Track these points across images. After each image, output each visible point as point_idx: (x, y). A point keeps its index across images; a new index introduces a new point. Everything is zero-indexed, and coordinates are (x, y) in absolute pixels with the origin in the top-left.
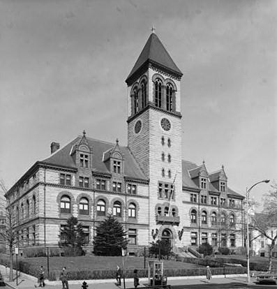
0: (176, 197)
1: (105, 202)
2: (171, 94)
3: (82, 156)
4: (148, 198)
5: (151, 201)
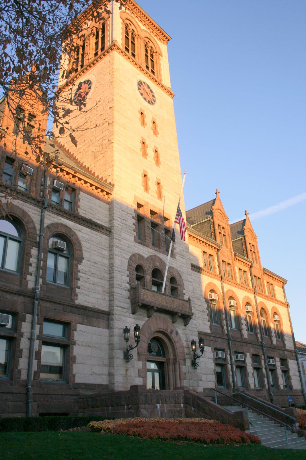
5: (116, 242)
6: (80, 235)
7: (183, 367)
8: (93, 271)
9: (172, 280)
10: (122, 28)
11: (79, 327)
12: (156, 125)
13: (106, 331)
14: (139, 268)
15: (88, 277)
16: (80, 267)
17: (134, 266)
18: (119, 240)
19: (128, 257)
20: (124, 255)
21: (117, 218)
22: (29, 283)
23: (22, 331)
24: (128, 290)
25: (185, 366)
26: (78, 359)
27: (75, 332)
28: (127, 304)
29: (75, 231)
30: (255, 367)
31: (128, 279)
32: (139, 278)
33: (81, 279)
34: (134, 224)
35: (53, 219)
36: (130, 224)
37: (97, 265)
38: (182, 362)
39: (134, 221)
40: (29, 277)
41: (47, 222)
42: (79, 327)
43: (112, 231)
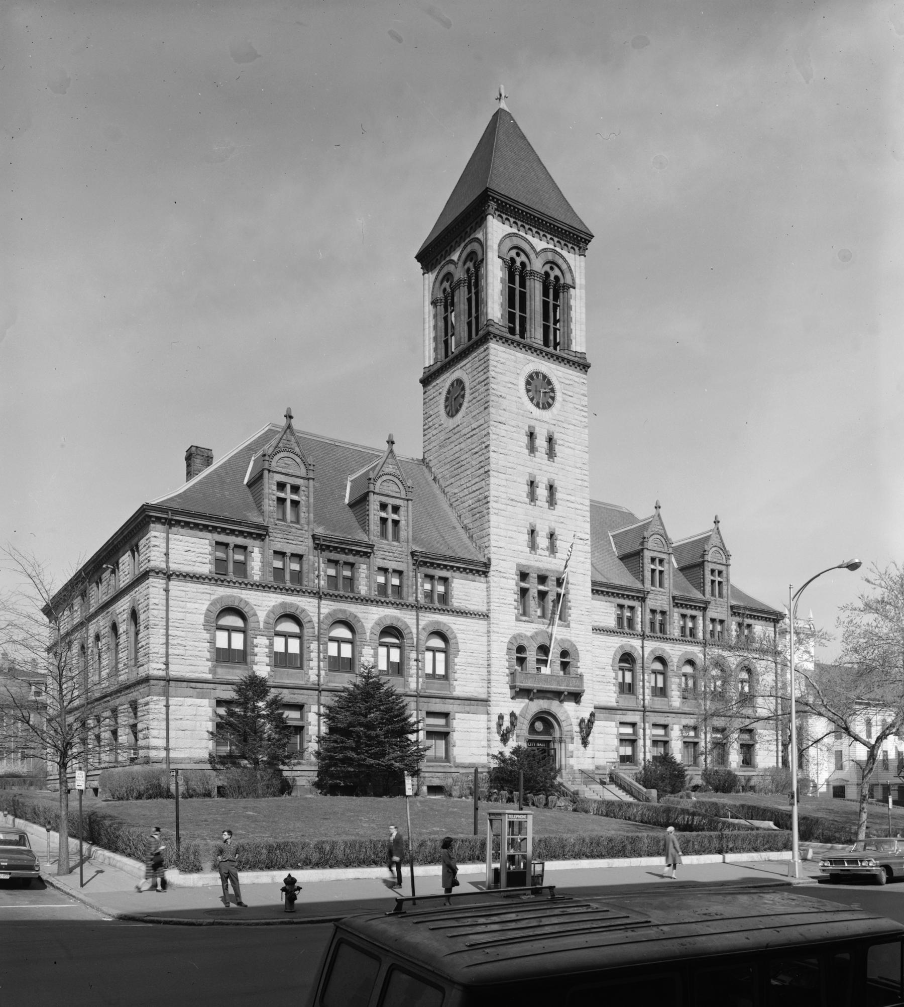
0: (574, 614)
1: (243, 617)
2: (556, 297)
3: (281, 486)
4: (486, 616)
5: (493, 628)
6: (454, 627)
7: (570, 745)
8: (470, 661)
9: (564, 654)
10: (502, 280)
11: (458, 716)
12: (452, 741)
13: (485, 717)
14: (521, 649)
15: (465, 668)
16: (456, 660)
17: (516, 645)
18: (497, 624)
19: (507, 640)
20: (502, 639)
21: (494, 600)
22: (411, 684)
23: (309, 720)
24: (507, 676)
25: (884, 782)
26: (458, 743)
27: (454, 748)
28: (508, 692)
29: (450, 625)
30: (744, 742)
31: (507, 664)
32: (521, 661)
33: (458, 671)
34: (515, 601)
35: (426, 619)
36: (510, 602)
37: (474, 655)
38: (568, 740)
39: (516, 597)
40: (410, 679)
41: (422, 623)
42: (458, 716)
43: (490, 615)
